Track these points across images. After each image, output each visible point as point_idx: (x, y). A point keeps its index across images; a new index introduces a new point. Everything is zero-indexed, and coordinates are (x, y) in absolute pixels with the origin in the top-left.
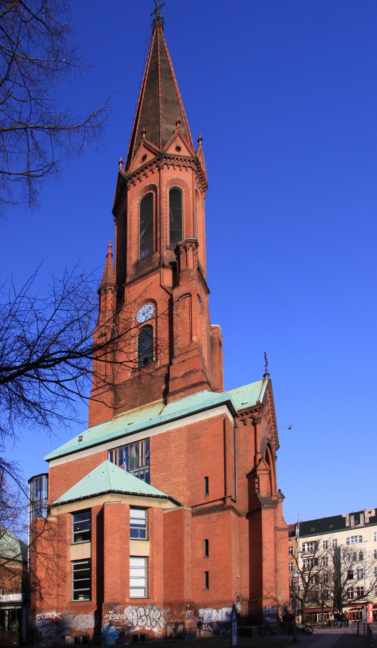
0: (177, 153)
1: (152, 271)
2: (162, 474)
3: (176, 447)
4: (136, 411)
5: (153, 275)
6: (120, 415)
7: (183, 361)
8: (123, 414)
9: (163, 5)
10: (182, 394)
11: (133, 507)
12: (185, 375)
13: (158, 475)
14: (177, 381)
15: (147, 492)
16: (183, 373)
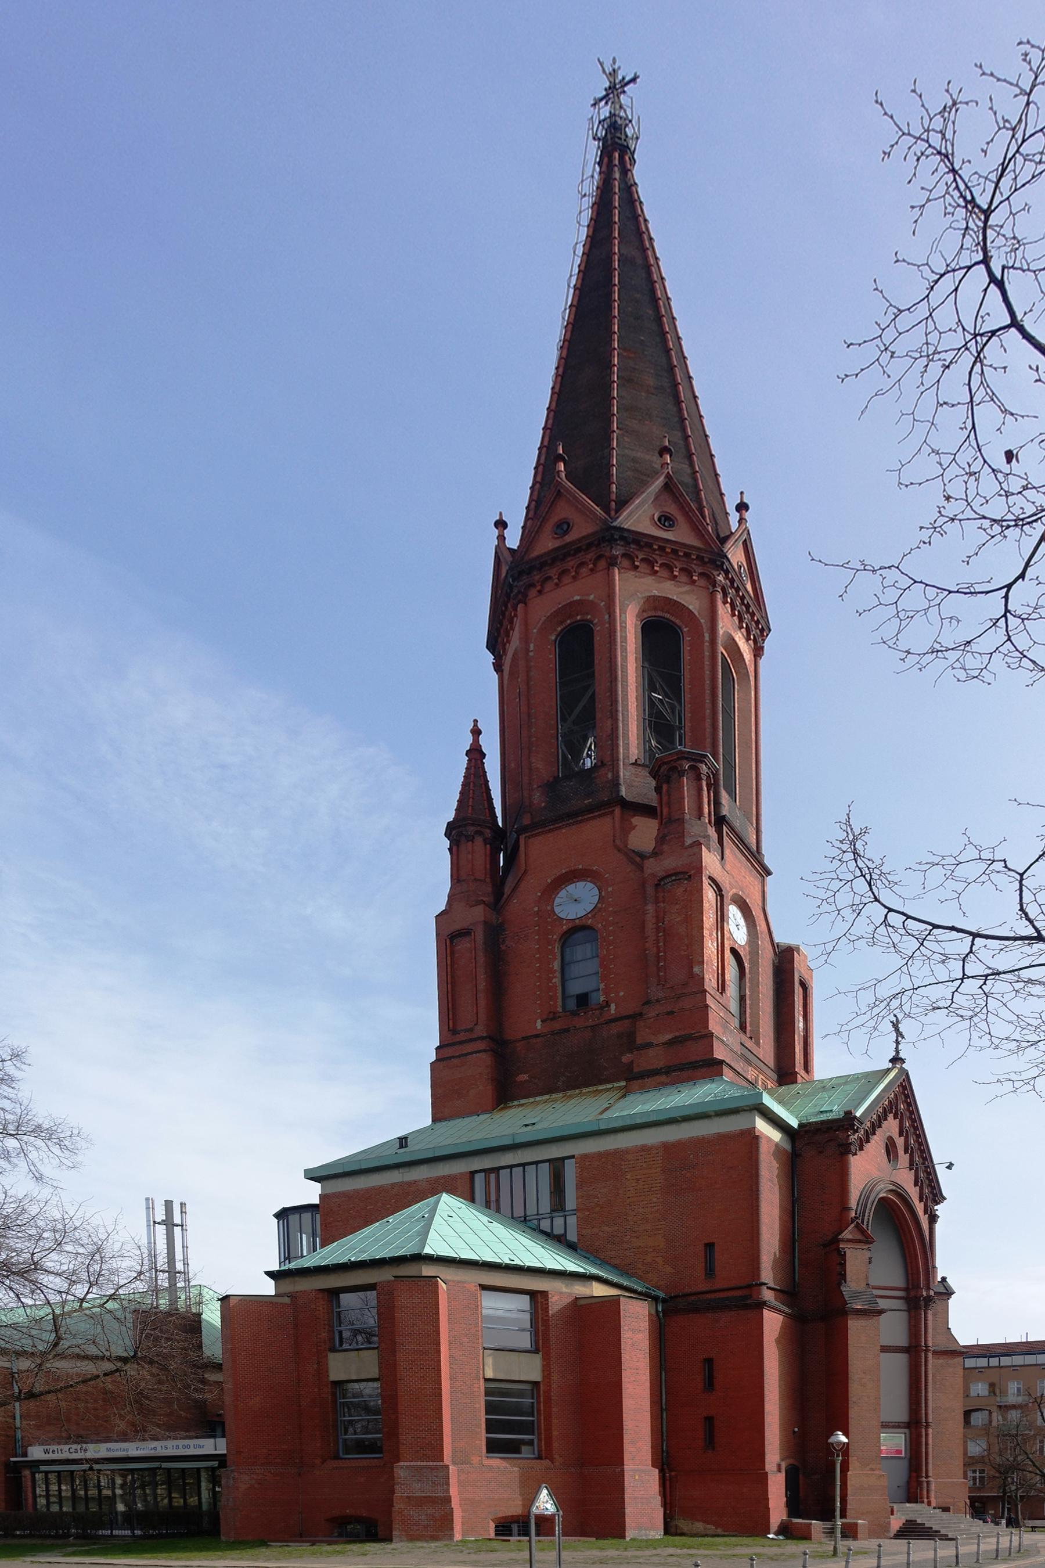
0: (554, 520)
1: (590, 809)
2: (606, 1229)
3: (638, 1180)
4: (556, 1100)
5: (594, 818)
6: (515, 1103)
7: (670, 1013)
8: (522, 1101)
9: (633, 80)
10: (663, 1078)
11: (484, 1287)
12: (670, 1043)
13: (596, 1230)
14: (651, 1052)
15: (530, 1262)
16: (668, 1037)
